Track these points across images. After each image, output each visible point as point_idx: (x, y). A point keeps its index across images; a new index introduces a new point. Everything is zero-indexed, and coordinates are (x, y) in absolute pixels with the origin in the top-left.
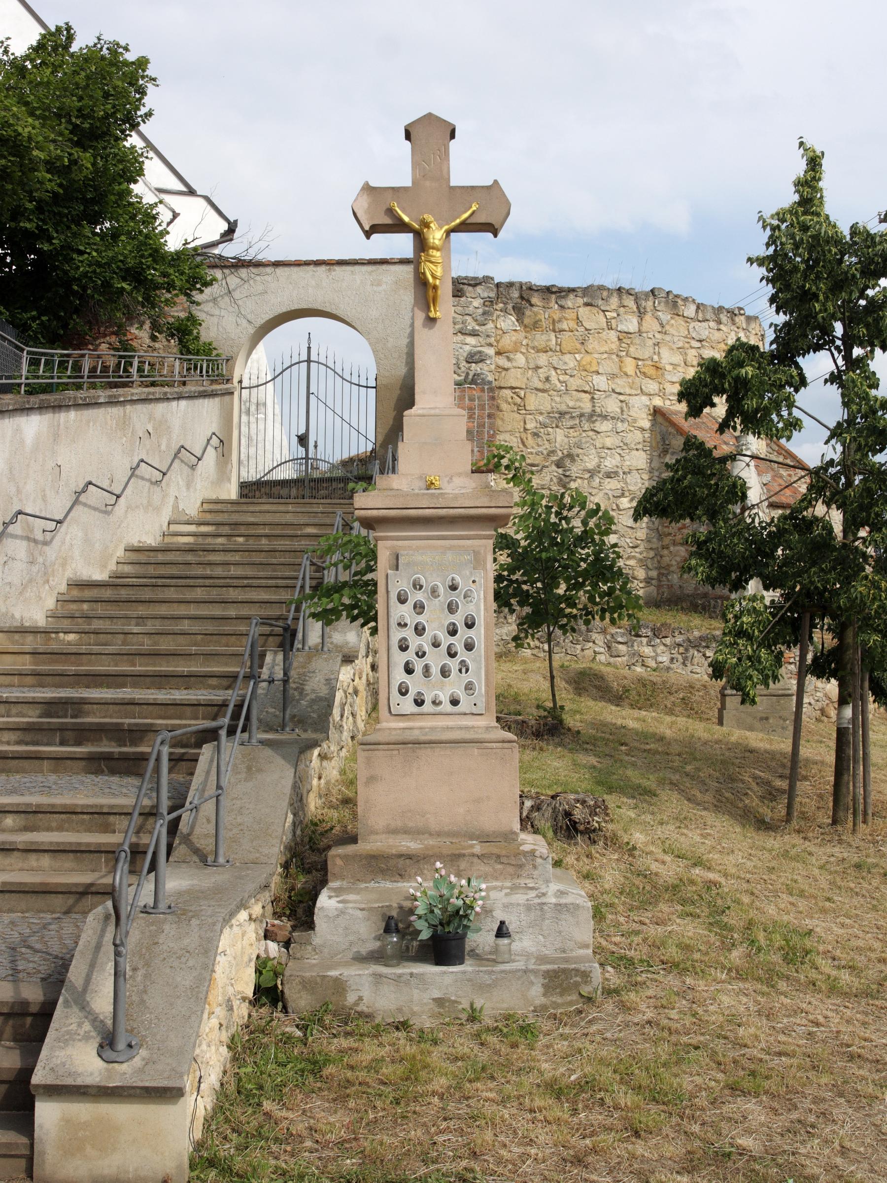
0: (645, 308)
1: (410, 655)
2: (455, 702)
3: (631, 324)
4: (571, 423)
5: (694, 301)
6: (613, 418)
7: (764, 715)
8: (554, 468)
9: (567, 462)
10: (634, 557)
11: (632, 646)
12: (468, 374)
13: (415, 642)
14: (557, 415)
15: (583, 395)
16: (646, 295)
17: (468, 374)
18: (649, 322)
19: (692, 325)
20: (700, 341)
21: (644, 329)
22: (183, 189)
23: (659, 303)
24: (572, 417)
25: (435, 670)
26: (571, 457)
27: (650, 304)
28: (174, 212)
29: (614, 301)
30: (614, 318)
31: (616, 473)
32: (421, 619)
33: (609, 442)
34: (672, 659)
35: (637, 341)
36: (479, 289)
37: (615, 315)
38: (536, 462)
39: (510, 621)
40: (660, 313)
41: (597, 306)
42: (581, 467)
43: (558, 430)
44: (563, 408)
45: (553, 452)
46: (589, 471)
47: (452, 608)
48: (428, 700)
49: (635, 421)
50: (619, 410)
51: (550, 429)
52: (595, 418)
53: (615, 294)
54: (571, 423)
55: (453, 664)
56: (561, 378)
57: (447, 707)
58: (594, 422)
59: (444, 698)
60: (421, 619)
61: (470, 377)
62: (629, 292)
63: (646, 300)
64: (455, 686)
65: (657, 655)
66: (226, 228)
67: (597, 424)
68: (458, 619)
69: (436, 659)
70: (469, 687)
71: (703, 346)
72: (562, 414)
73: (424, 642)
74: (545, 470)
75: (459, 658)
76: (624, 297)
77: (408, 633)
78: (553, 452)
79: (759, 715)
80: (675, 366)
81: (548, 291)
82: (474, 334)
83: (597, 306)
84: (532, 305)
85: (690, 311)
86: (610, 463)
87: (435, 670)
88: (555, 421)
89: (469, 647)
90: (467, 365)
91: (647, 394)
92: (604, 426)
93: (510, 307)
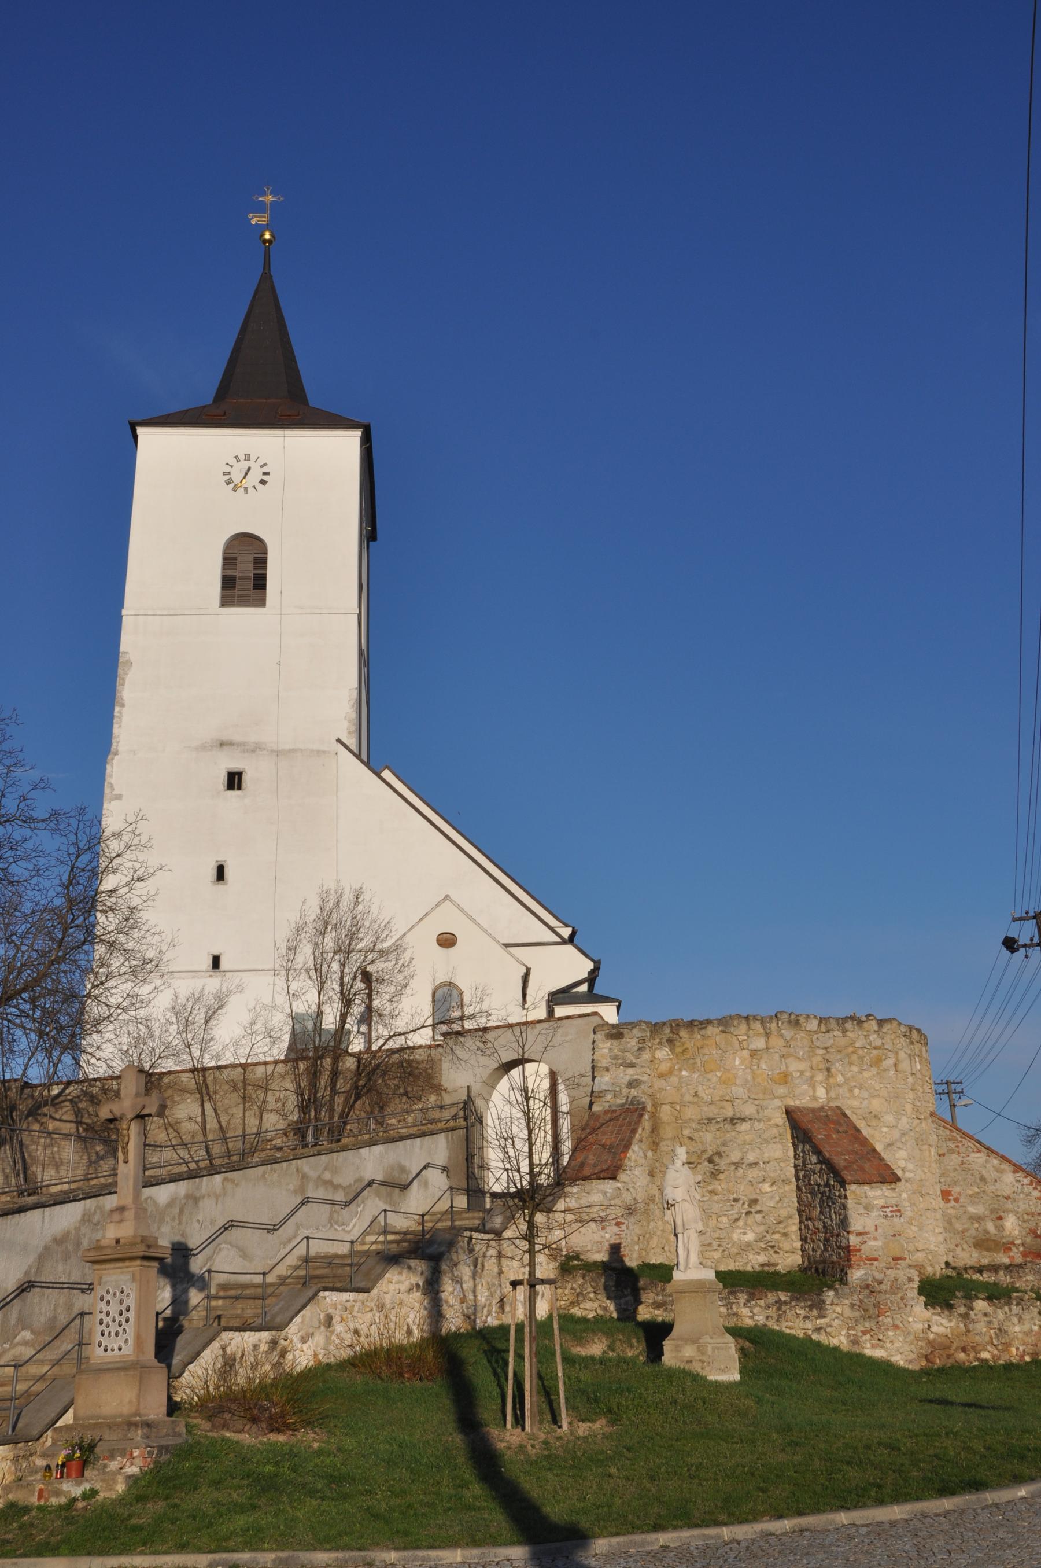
0: (770, 1029)
1: (103, 1327)
2: (120, 1349)
3: (760, 1043)
4: (718, 1126)
5: (815, 1017)
6: (751, 1119)
7: (689, 1359)
8: (706, 1163)
9: (716, 1159)
10: (778, 1232)
11: (731, 1308)
12: (628, 1097)
13: (106, 1320)
14: (706, 1122)
15: (725, 1103)
16: (771, 1018)
17: (628, 1097)
18: (776, 1042)
19: (815, 1037)
20: (826, 1048)
21: (770, 1045)
22: (559, 940)
23: (782, 1023)
24: (718, 1122)
25: (113, 1334)
26: (719, 1154)
27: (774, 1025)
28: (527, 967)
29: (743, 1027)
30: (745, 1040)
31: (756, 1164)
32: (109, 1308)
33: (748, 1138)
34: (767, 1317)
35: (765, 1056)
36: (636, 1031)
37: (746, 1038)
38: (692, 1161)
39: (626, 1293)
40: (783, 1032)
41: (730, 1033)
42: (728, 1162)
43: (707, 1133)
44: (711, 1115)
45: (704, 1151)
46: (734, 1164)
47: (121, 1302)
48: (109, 1349)
49: (769, 1120)
50: (755, 1112)
51: (701, 1134)
52: (736, 1121)
53: (743, 1021)
54: (718, 1126)
55: (120, 1330)
56: (707, 1092)
57: (116, 1352)
58: (734, 1124)
59: (116, 1348)
60: (109, 1308)
61: (629, 1100)
62: (755, 1018)
63: (771, 1022)
64: (120, 1341)
65: (754, 1315)
66: (592, 967)
67: (738, 1125)
68: (123, 1308)
69: (113, 1328)
70: (126, 1341)
71: (828, 1052)
72: (710, 1120)
73: (109, 1319)
74: (700, 1166)
75: (122, 1327)
76: (752, 1022)
77: (103, 1316)
78: (704, 1151)
79: (685, 1359)
80: (802, 1073)
81: (691, 1024)
82: (632, 1065)
83: (730, 1033)
84: (680, 1038)
85: (813, 1025)
86: (751, 1157)
87: (113, 1334)
88: (705, 1127)
89: (127, 1321)
90: (628, 1091)
91: (778, 1098)
92: (744, 1127)
93: (664, 1040)
